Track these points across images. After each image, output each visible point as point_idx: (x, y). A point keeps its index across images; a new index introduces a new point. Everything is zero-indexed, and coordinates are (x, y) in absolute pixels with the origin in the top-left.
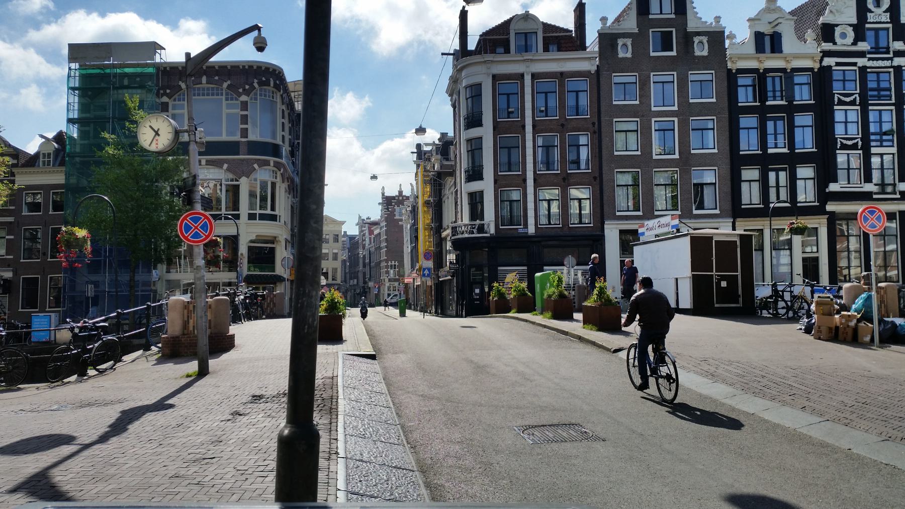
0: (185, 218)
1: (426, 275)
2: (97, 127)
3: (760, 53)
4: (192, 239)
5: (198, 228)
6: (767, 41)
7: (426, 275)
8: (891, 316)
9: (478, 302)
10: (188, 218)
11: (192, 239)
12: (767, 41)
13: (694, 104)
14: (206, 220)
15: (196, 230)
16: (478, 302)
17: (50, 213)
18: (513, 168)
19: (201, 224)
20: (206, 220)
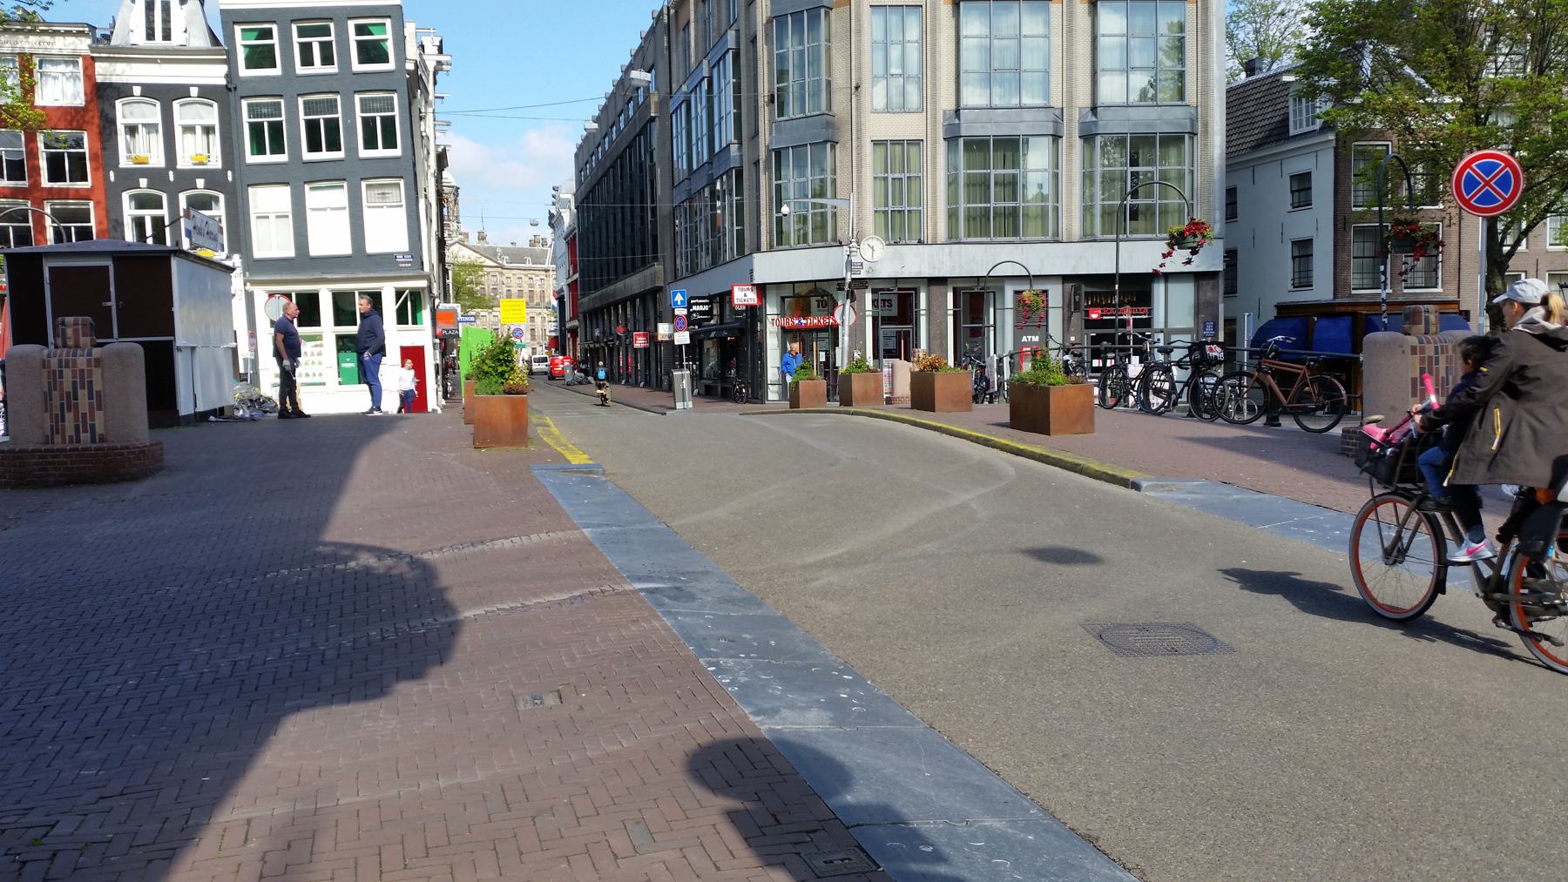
0: (1507, 202)
1: (679, 303)
2: (640, 342)
3: (150, 40)
4: (1465, 175)
5: (1483, 183)
6: (592, 287)
7: (679, 303)
8: (109, 304)
9: (230, 179)
10: (1502, 201)
11: (1465, 175)
12: (592, 287)
13: (260, 48)
14: (1467, 198)
15: (1488, 179)
16: (230, 179)
17: (1083, 286)
18: (1040, 208)
19: (1493, 192)
20: (1467, 198)
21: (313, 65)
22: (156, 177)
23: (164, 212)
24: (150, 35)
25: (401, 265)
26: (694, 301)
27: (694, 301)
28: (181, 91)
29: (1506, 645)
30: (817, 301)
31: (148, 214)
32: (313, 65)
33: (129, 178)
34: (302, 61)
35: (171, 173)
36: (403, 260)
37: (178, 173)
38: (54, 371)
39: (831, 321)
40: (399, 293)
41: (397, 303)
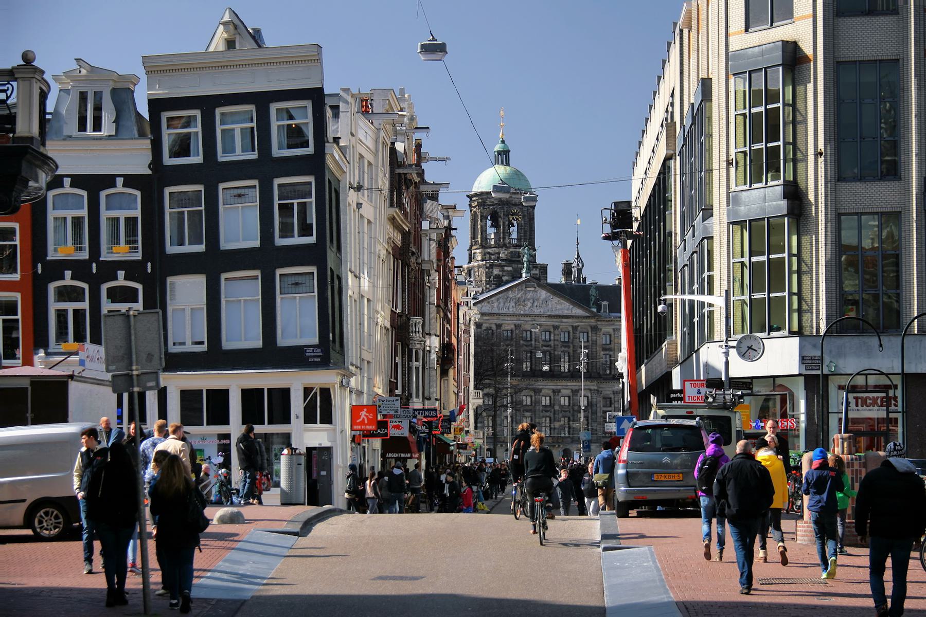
21: (74, 310)
22: (79, 269)
23: (85, 305)
24: (82, 127)
25: (311, 360)
26: (675, 396)
27: (675, 396)
28: (108, 181)
29: (237, 535)
30: (854, 398)
31: (70, 306)
32: (74, 310)
33: (56, 269)
34: (67, 314)
35: (94, 265)
36: (312, 354)
37: (101, 264)
38: (864, 467)
39: (790, 424)
40: (307, 391)
41: (304, 402)
